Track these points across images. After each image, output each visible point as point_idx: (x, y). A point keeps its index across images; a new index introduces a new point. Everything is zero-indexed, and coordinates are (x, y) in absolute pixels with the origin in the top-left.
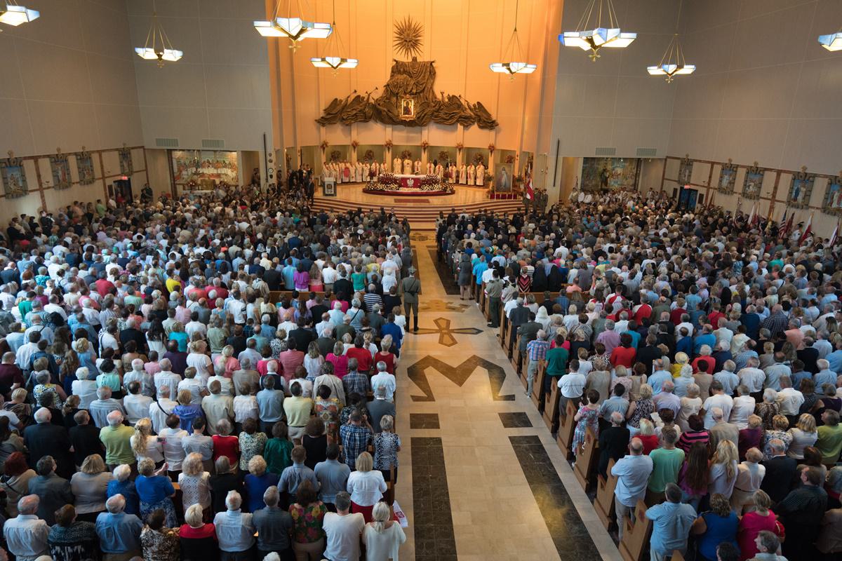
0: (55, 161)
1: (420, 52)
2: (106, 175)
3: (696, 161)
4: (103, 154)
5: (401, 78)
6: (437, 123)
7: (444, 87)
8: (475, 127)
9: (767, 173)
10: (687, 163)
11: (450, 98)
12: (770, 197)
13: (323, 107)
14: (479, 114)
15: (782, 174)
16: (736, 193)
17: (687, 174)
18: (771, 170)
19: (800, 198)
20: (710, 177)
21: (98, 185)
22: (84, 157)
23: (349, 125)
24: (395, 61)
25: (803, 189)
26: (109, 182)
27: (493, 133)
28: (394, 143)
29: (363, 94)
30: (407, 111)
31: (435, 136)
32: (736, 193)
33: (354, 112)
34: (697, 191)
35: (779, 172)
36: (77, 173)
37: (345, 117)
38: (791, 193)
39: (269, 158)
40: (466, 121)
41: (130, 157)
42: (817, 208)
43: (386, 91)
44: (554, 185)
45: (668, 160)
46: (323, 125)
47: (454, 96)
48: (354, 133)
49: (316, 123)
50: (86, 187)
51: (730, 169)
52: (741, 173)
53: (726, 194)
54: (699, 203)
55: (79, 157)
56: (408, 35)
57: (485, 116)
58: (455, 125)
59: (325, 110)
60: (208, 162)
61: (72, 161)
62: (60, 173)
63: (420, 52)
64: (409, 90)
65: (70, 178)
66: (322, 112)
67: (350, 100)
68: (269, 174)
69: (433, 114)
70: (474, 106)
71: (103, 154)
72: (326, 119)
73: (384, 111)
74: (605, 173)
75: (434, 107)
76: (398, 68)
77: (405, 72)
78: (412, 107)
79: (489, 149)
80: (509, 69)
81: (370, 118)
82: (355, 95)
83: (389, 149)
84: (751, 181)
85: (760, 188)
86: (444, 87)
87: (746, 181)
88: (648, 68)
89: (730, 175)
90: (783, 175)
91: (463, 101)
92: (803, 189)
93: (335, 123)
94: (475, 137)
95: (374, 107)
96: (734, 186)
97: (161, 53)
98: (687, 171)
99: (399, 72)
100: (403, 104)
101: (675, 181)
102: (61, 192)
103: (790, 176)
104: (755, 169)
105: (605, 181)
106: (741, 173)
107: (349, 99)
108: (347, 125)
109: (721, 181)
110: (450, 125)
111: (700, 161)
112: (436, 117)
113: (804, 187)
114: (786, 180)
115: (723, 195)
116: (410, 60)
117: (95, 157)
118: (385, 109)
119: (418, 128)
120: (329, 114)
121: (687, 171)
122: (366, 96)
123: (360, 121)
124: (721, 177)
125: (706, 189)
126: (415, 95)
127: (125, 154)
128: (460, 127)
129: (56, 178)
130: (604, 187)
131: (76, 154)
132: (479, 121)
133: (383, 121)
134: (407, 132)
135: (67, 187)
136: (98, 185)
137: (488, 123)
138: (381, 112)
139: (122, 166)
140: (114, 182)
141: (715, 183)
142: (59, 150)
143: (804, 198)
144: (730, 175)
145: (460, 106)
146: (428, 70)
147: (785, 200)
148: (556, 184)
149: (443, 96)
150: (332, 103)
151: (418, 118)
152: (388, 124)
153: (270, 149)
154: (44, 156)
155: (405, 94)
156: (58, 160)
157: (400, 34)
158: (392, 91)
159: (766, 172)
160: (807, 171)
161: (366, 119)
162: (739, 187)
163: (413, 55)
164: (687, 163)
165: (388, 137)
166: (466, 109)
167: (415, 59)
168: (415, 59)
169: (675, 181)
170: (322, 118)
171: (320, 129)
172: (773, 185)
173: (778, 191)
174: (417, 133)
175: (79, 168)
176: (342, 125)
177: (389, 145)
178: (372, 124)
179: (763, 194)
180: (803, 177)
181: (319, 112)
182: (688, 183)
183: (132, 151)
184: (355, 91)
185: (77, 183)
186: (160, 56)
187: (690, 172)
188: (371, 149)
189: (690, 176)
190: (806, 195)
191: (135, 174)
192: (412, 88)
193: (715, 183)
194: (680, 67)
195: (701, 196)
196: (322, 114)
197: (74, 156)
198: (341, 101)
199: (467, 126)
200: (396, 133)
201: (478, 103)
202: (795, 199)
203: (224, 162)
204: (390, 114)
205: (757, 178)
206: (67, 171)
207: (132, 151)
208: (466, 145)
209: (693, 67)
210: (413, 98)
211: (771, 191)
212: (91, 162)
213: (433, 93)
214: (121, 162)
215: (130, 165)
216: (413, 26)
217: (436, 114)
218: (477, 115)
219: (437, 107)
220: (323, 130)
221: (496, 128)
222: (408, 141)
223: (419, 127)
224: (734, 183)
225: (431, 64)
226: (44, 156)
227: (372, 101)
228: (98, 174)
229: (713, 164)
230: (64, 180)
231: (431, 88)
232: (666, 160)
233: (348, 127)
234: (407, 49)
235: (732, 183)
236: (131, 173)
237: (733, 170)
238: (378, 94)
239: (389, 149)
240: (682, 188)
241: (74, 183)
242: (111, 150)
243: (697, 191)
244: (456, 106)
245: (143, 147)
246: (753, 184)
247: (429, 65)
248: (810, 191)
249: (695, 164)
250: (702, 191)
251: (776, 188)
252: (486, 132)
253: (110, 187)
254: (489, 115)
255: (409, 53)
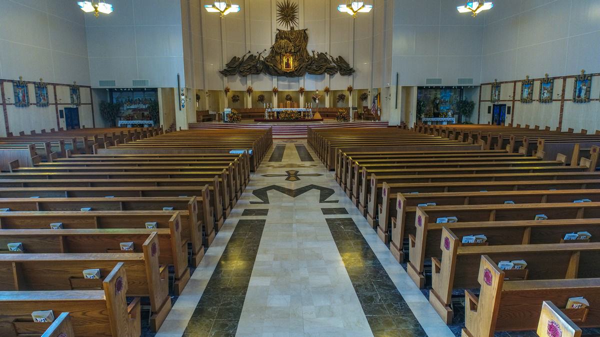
0: (17, 86)
1: (296, 23)
2: (58, 102)
3: (502, 83)
4: (57, 87)
5: (283, 42)
6: (310, 73)
7: (315, 46)
8: (338, 75)
9: (555, 81)
10: (496, 86)
11: (318, 55)
12: (560, 98)
13: (225, 62)
14: (340, 65)
15: (567, 79)
16: (534, 100)
17: (497, 94)
18: (559, 78)
19: (583, 95)
20: (514, 93)
21: (52, 108)
22: (41, 87)
23: (245, 76)
24: (278, 30)
25: (584, 88)
26: (60, 108)
27: (351, 78)
28: (280, 90)
29: (255, 54)
30: (288, 65)
31: (309, 83)
32: (534, 100)
33: (249, 67)
34: (505, 105)
35: (565, 78)
36: (35, 97)
37: (242, 70)
38: (575, 92)
39: (181, 92)
40: (331, 71)
41: (79, 93)
42: (597, 100)
43: (272, 52)
44: (396, 108)
45: (483, 86)
46: (226, 76)
47: (321, 53)
48: (249, 83)
49: (219, 73)
50: (41, 109)
51: (528, 83)
52: (537, 85)
53: (527, 102)
54: (508, 114)
55: (37, 86)
56: (287, 12)
57: (345, 65)
58: (323, 76)
59: (227, 65)
60: (139, 100)
61: (31, 89)
62: (21, 95)
63: (296, 23)
64: (289, 50)
65: (28, 100)
66: (224, 66)
67: (245, 58)
68: (182, 104)
69: (307, 67)
70: (337, 59)
71: (57, 87)
72: (228, 71)
73: (271, 66)
74: (436, 101)
75: (308, 62)
76: (280, 35)
77: (285, 38)
78: (291, 63)
79: (348, 90)
80: (352, 9)
81: (261, 71)
82: (249, 54)
83: (275, 94)
84: (545, 89)
85: (552, 93)
86: (315, 46)
87: (541, 90)
88: (458, 8)
89: (529, 88)
90: (568, 80)
91: (328, 57)
92: (584, 88)
93: (235, 75)
94: (339, 83)
95: (263, 63)
96: (532, 95)
97: (96, 6)
98: (497, 91)
99: (282, 38)
100: (285, 60)
101: (489, 101)
102: (21, 109)
103: (573, 80)
104: (546, 80)
105: (436, 106)
106: (537, 85)
107: (245, 57)
108: (244, 76)
109: (522, 94)
110: (320, 74)
111: (506, 82)
112: (309, 69)
113: (585, 85)
114: (570, 83)
115: (525, 104)
116: (289, 29)
117: (50, 88)
118: (272, 65)
119: (296, 78)
120: (229, 67)
121: (497, 91)
122: (257, 55)
123: (254, 74)
124: (522, 91)
125: (512, 102)
126: (294, 54)
127: (75, 89)
128: (327, 76)
129: (17, 97)
130: (436, 111)
131: (34, 83)
132: (341, 70)
133: (271, 74)
134: (289, 82)
135: (25, 106)
136: (52, 108)
137: (345, 69)
138: (268, 67)
139: (72, 98)
140: (65, 108)
141: (518, 97)
142: (20, 78)
143: (585, 94)
144: (529, 88)
145: (326, 60)
146: (303, 36)
147: (572, 98)
148: (398, 106)
149: (314, 54)
150: (232, 59)
151: (296, 70)
152: (275, 75)
153: (183, 85)
154: (9, 81)
155: (286, 53)
156: (20, 85)
157: (281, 11)
158: (276, 52)
159: (555, 80)
160: (585, 74)
161: (258, 72)
162: (536, 96)
163: (291, 25)
164: (496, 86)
165: (275, 85)
166: (331, 62)
167: (292, 28)
168: (292, 28)
169: (489, 101)
170: (225, 70)
171: (223, 80)
172: (562, 89)
173: (566, 93)
174: (295, 82)
175: (36, 93)
176: (240, 76)
177: (275, 91)
178: (262, 75)
179: (555, 97)
180: (583, 78)
181: (223, 66)
182: (499, 100)
183: (81, 88)
184: (250, 52)
185: (34, 104)
186: (96, 8)
187: (499, 92)
188: (262, 94)
189: (499, 95)
190: (587, 91)
191: (82, 106)
192: (291, 49)
193: (518, 97)
194: (481, 4)
195: (509, 108)
196: (225, 67)
197: (34, 85)
198: (239, 58)
199: (332, 75)
200: (281, 83)
201: (340, 57)
202: (579, 96)
203: (150, 99)
204: (275, 68)
205: (548, 87)
206: (25, 95)
207: (81, 88)
208: (332, 89)
209: (491, 3)
210: (292, 56)
211: (560, 93)
212: (47, 91)
213: (307, 52)
214: (71, 95)
215: (79, 98)
216: (290, 6)
217: (309, 67)
218: (339, 66)
219: (310, 62)
220: (225, 79)
221: (354, 74)
222: (289, 88)
223: (297, 78)
224: (532, 94)
225: (305, 32)
226: (9, 81)
227: (262, 59)
228: (51, 100)
229: (515, 82)
230: (24, 100)
231: (305, 48)
232: (481, 87)
233: (245, 78)
234: (287, 22)
235: (531, 94)
236: (79, 104)
237: (530, 84)
238: (266, 55)
239: (275, 94)
240: (494, 105)
241: (31, 104)
242: (64, 85)
243: (505, 105)
244: (323, 60)
245: (90, 87)
246: (546, 91)
247: (303, 32)
248: (590, 87)
249: (502, 85)
250: (510, 104)
251: (564, 91)
252: (346, 77)
253: (61, 111)
254: (348, 65)
255: (289, 25)
